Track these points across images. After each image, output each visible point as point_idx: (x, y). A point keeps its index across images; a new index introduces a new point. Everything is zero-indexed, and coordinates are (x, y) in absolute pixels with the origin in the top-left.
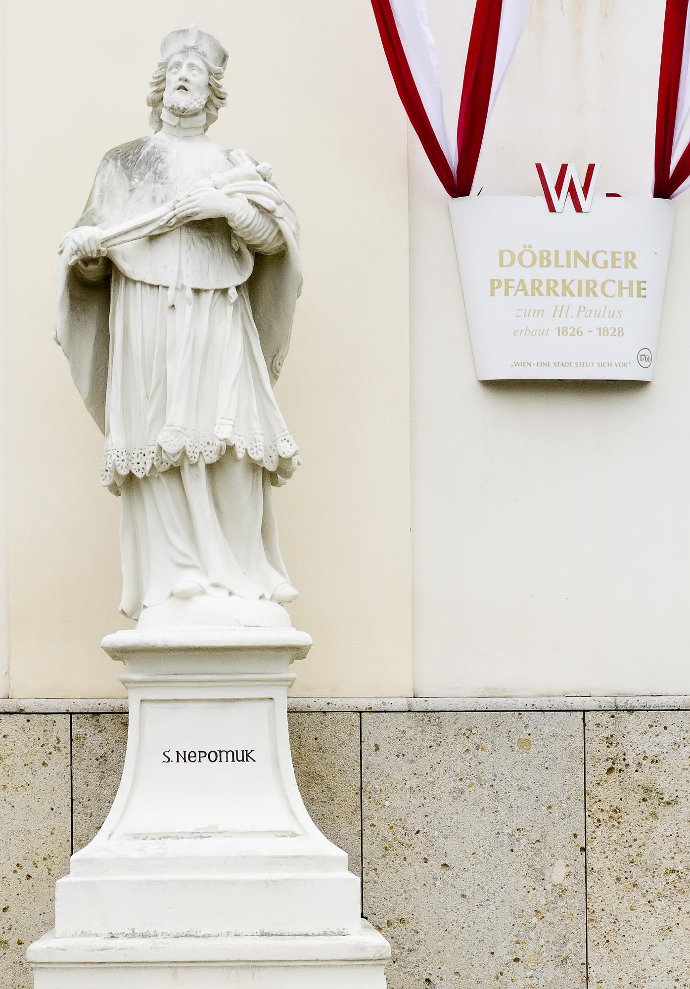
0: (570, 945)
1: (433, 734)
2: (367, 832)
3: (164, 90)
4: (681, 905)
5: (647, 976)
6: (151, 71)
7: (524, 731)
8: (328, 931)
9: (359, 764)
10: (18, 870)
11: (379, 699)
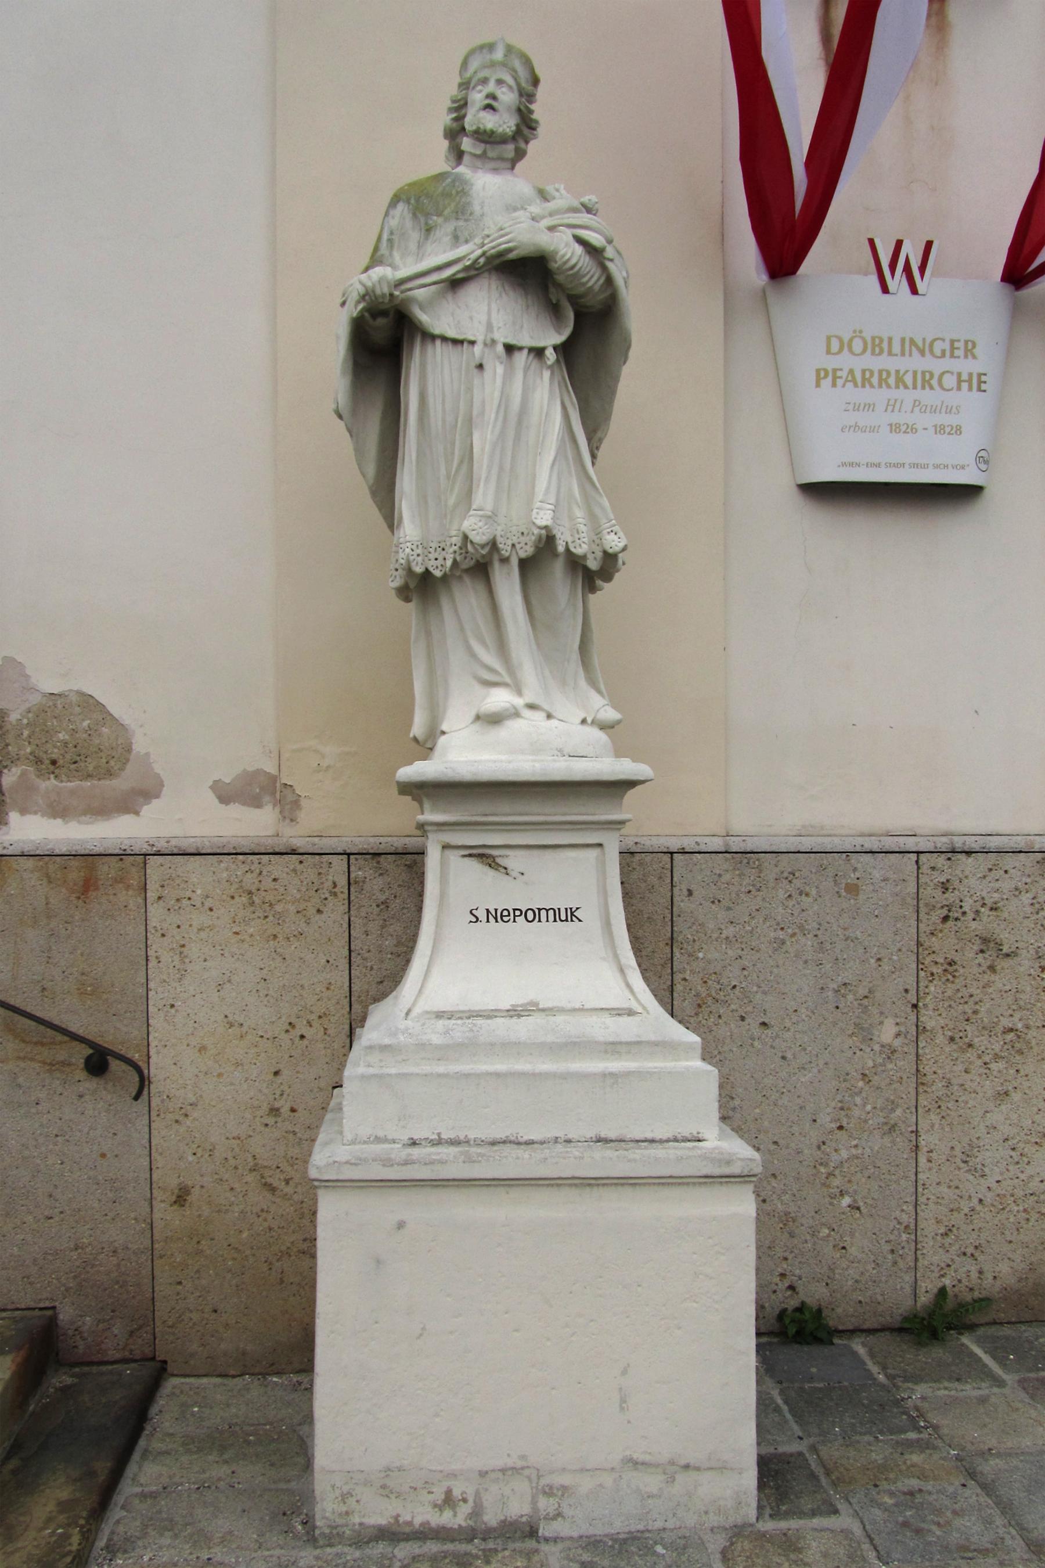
0: (899, 1112)
1: (752, 878)
2: (678, 988)
3: (464, 116)
4: (1019, 1067)
5: (981, 1144)
6: (451, 89)
7: (852, 875)
8: (679, 1136)
9: (670, 911)
10: (291, 1030)
11: (692, 839)
